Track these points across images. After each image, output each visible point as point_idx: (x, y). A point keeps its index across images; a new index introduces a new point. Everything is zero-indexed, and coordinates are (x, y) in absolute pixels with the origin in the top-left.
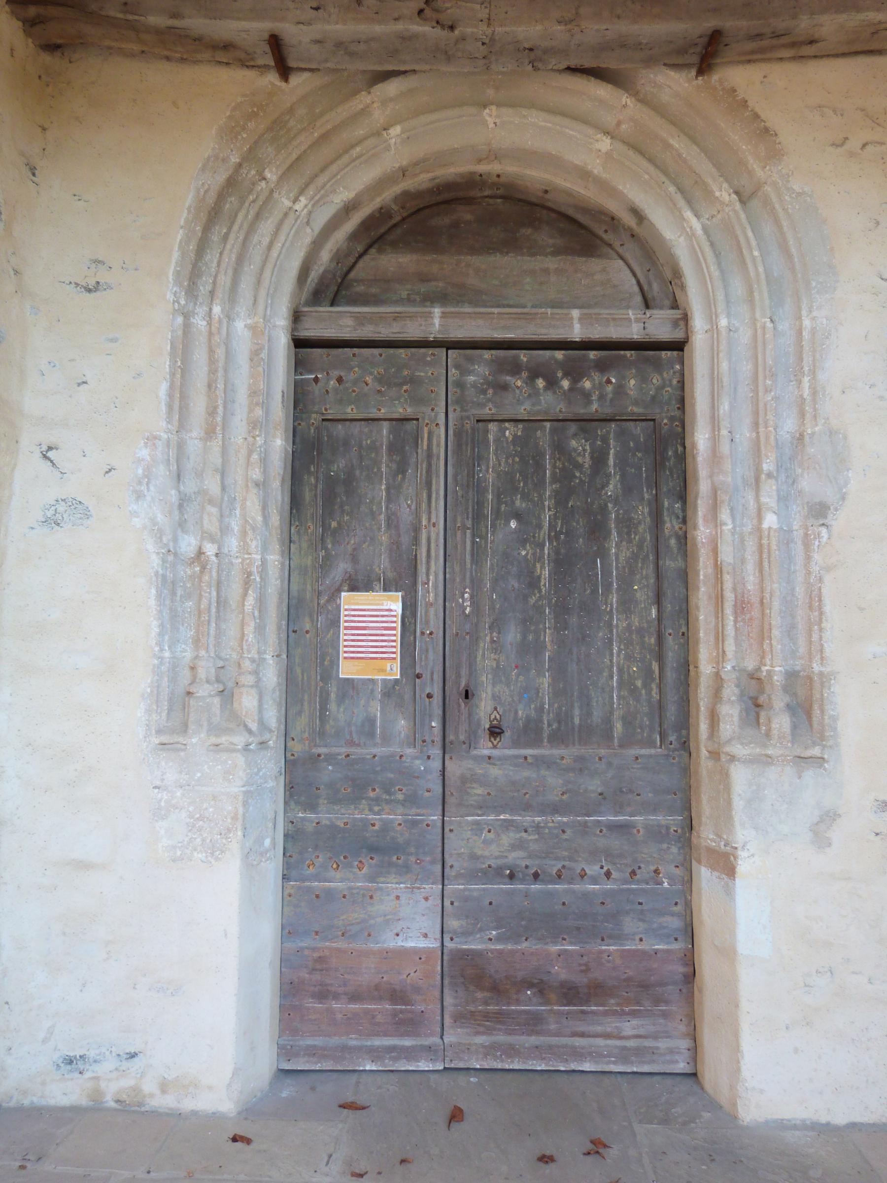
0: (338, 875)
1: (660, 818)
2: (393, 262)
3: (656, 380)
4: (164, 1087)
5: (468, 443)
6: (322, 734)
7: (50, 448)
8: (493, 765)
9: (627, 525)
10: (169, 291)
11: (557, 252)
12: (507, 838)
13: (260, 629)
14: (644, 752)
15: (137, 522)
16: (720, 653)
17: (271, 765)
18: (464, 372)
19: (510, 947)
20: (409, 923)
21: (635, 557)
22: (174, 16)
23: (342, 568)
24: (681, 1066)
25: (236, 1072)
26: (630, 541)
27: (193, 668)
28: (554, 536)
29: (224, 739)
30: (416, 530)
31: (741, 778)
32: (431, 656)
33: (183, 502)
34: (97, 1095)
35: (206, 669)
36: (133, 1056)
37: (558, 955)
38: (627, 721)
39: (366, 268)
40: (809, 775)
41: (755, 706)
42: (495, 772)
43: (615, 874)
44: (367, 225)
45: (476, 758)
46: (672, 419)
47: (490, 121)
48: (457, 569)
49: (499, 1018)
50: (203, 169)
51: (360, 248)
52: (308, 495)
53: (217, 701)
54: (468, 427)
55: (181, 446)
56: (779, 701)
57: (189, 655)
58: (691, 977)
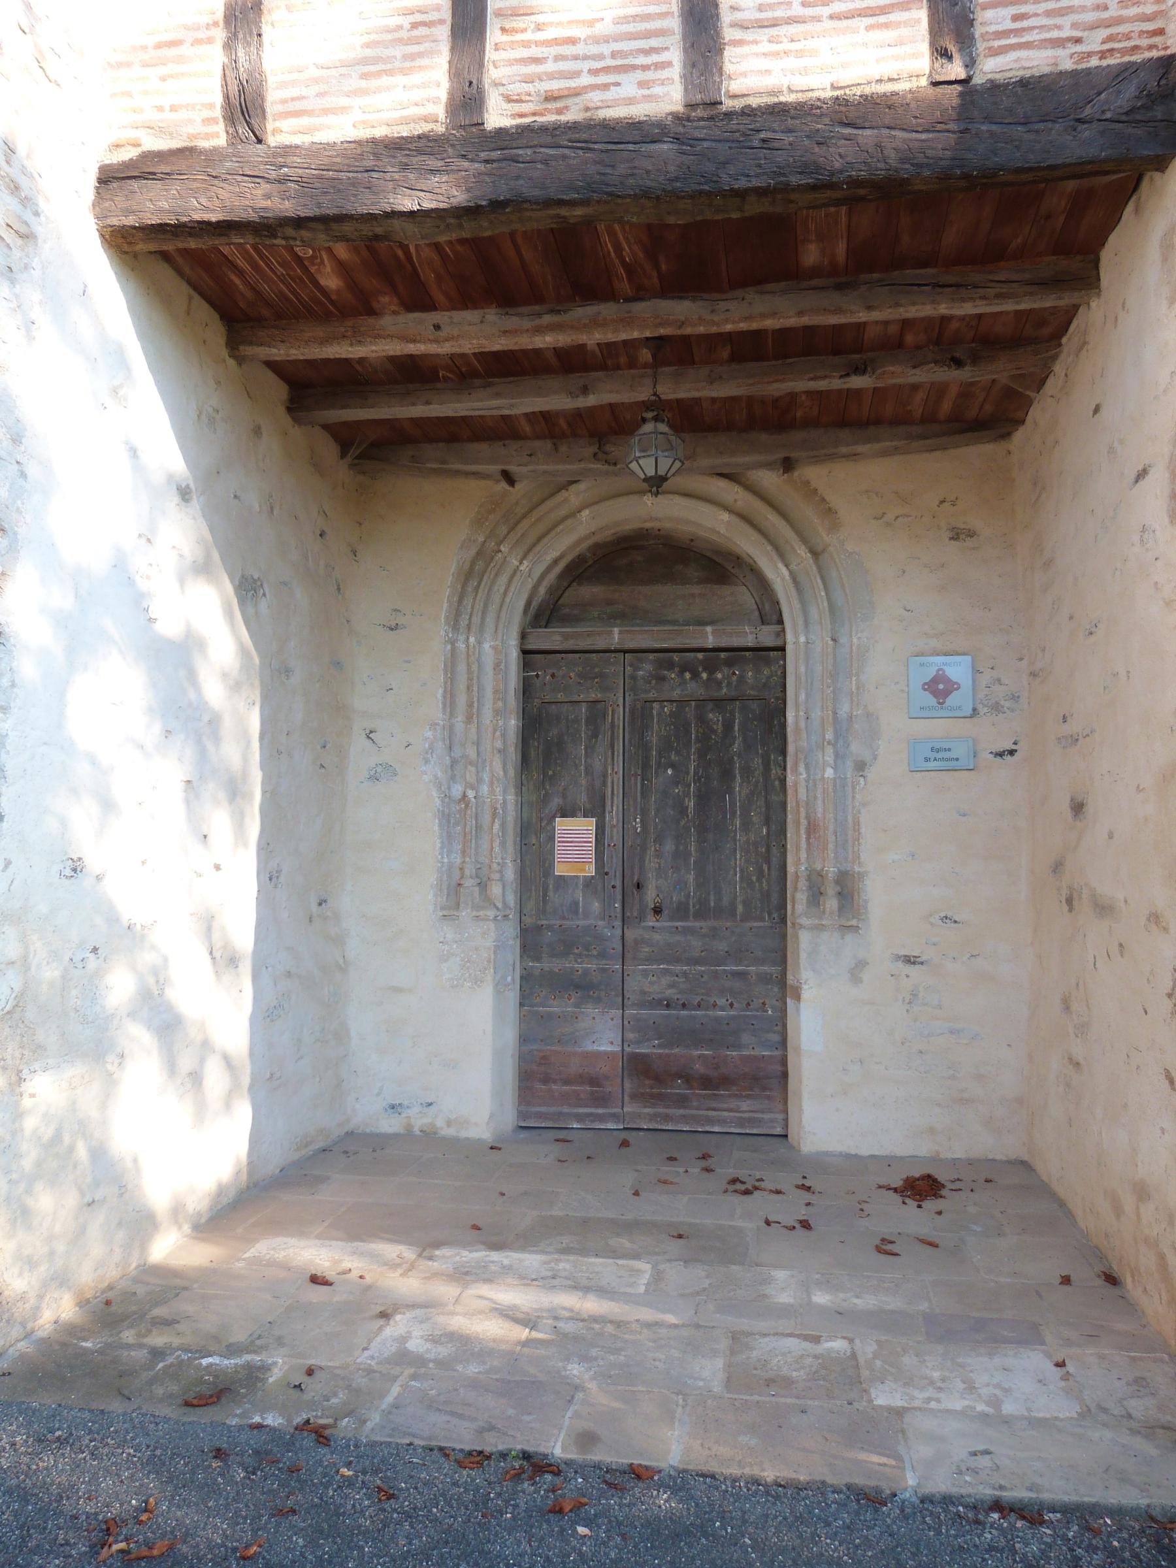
0: (555, 1003)
1: (765, 968)
2: (587, 591)
3: (766, 672)
4: (449, 1123)
5: (640, 718)
6: (544, 912)
7: (371, 732)
8: (656, 932)
9: (747, 771)
10: (442, 629)
11: (701, 582)
12: (665, 981)
13: (503, 844)
14: (755, 924)
15: (426, 778)
16: (799, 860)
17: (511, 931)
18: (636, 669)
19: (667, 1051)
20: (602, 1035)
21: (752, 793)
22: (443, 463)
23: (556, 802)
24: (778, 1130)
25: (492, 1116)
26: (749, 782)
27: (461, 869)
28: (698, 778)
29: (481, 913)
30: (605, 776)
31: (805, 940)
32: (614, 860)
33: (454, 763)
34: (409, 1127)
35: (469, 870)
36: (430, 1104)
37: (698, 1056)
38: (746, 903)
39: (569, 597)
40: (849, 937)
41: (816, 896)
42: (657, 937)
43: (736, 1005)
44: (569, 568)
45: (644, 928)
46: (777, 699)
47: (649, 503)
48: (631, 802)
49: (660, 1098)
50: (461, 548)
51: (565, 584)
52: (533, 754)
53: (477, 889)
54: (639, 706)
55: (451, 728)
56: (831, 890)
57: (459, 861)
58: (785, 1075)
